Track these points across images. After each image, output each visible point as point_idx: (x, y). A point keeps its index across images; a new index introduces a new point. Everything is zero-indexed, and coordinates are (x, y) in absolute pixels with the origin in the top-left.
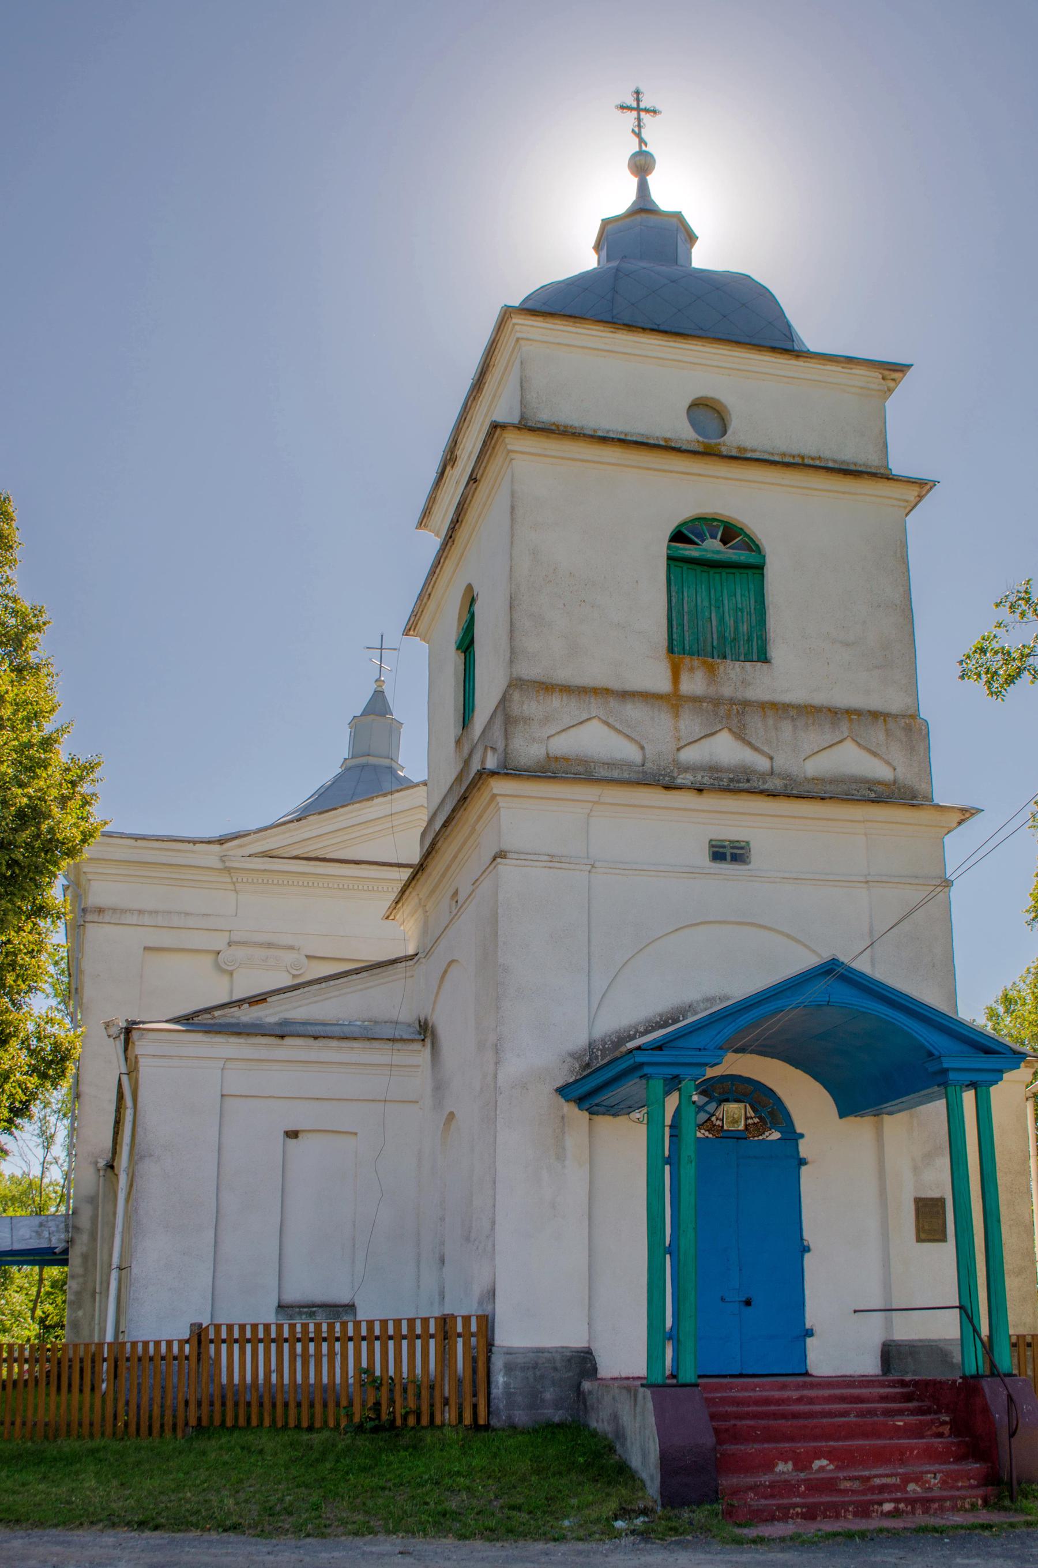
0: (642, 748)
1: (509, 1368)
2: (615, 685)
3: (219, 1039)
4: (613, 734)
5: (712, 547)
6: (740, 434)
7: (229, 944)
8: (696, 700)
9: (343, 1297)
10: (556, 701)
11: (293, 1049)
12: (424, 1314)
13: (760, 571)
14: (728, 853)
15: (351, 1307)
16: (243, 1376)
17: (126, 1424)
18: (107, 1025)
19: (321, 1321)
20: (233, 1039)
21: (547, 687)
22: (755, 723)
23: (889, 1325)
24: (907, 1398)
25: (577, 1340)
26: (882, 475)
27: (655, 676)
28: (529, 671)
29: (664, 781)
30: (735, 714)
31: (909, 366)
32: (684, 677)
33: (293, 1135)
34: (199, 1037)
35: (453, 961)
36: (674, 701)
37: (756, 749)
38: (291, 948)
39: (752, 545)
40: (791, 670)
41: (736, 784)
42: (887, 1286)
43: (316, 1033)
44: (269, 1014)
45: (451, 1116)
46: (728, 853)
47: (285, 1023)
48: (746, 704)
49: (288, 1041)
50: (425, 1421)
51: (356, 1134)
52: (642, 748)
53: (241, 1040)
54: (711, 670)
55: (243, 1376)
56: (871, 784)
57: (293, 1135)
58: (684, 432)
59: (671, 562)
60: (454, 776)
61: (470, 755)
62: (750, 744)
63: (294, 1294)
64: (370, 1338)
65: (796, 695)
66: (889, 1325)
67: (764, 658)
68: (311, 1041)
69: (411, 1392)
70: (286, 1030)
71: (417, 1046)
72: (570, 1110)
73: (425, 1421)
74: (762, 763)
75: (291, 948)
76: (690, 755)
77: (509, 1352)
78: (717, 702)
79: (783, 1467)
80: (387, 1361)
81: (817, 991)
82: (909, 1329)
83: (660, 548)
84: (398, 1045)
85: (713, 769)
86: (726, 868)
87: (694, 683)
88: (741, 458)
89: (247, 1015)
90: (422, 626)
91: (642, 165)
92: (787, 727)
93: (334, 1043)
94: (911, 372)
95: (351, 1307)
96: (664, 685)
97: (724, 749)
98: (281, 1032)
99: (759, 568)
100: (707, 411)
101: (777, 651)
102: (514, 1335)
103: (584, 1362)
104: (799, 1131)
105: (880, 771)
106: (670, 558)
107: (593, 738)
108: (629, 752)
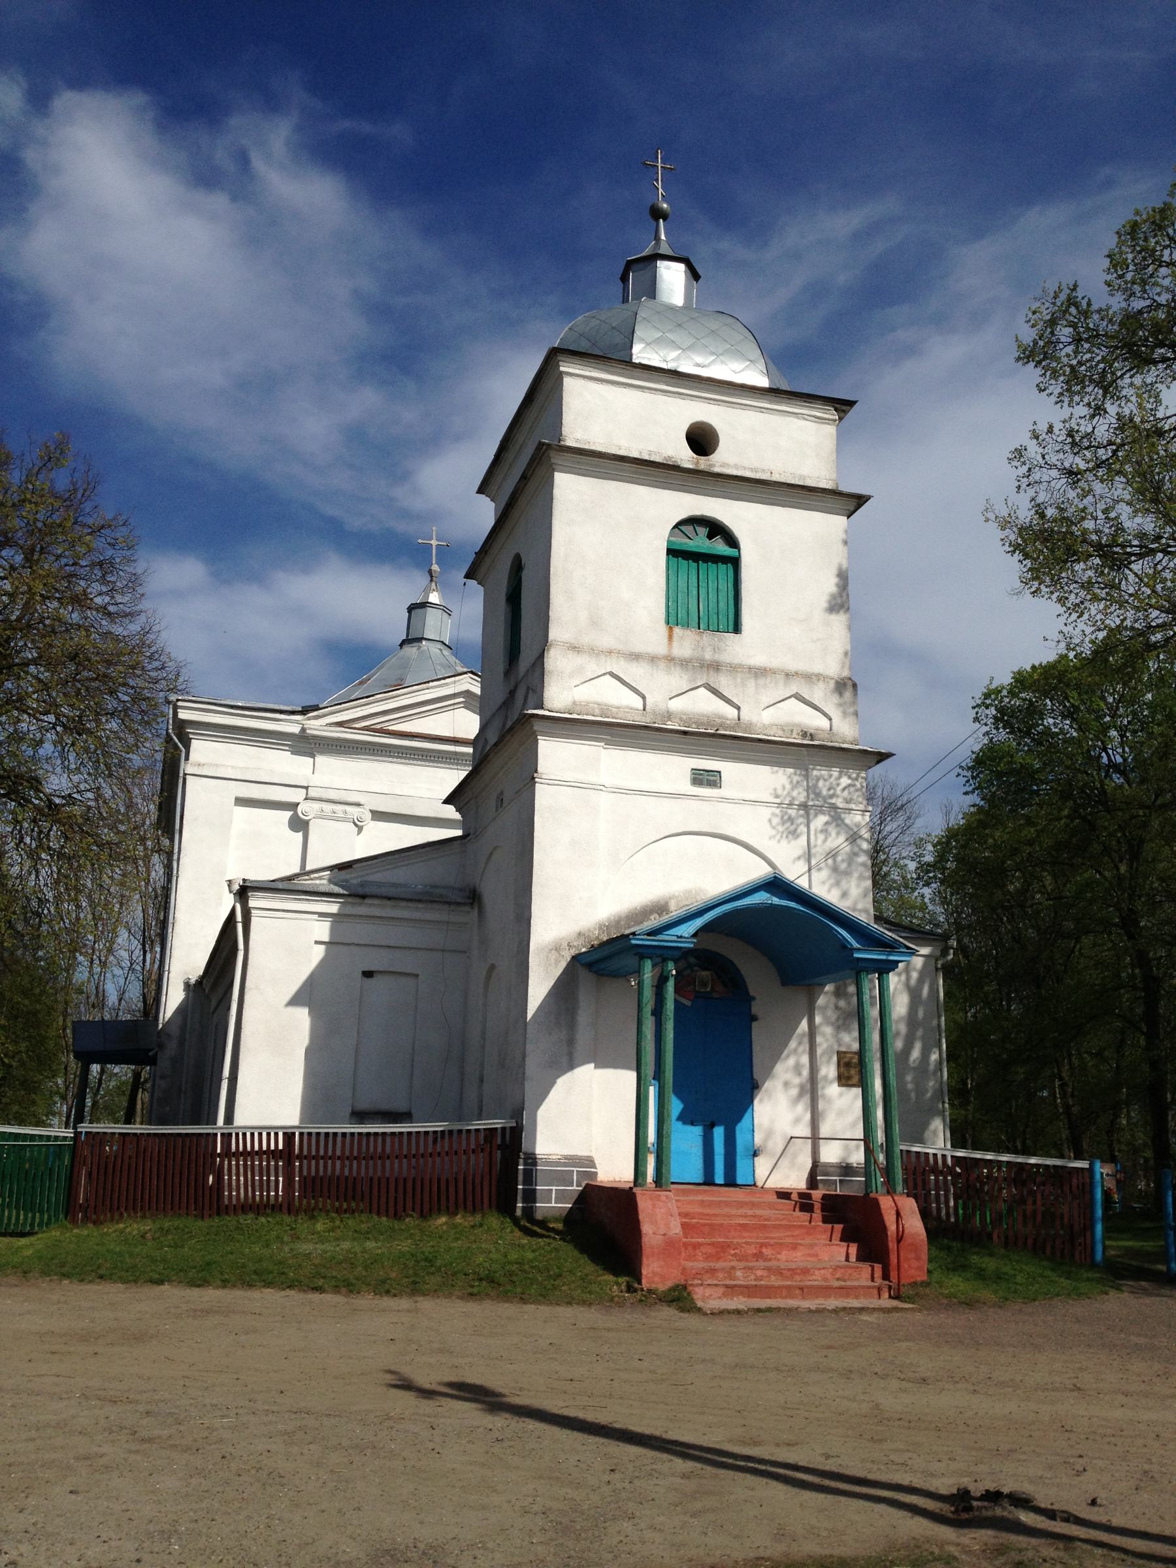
0: (644, 698)
5: (700, 542)
6: (724, 459)
7: (306, 799)
13: (731, 628)
14: (705, 779)
18: (230, 883)
22: (724, 683)
30: (707, 670)
31: (855, 402)
32: (675, 644)
35: (495, 848)
38: (358, 805)
39: (732, 542)
45: (492, 967)
49: (368, 901)
51: (417, 976)
52: (644, 698)
55: (359, 1172)
57: (368, 974)
58: (685, 456)
59: (673, 560)
60: (502, 700)
61: (516, 687)
63: (363, 1105)
65: (759, 659)
70: (367, 890)
71: (467, 908)
75: (358, 805)
76: (676, 705)
80: (227, 1101)
81: (762, 897)
84: (452, 907)
87: (687, 643)
90: (481, 572)
92: (751, 683)
93: (403, 904)
94: (856, 407)
97: (701, 705)
99: (735, 562)
100: (701, 439)
104: (752, 994)
106: (672, 552)
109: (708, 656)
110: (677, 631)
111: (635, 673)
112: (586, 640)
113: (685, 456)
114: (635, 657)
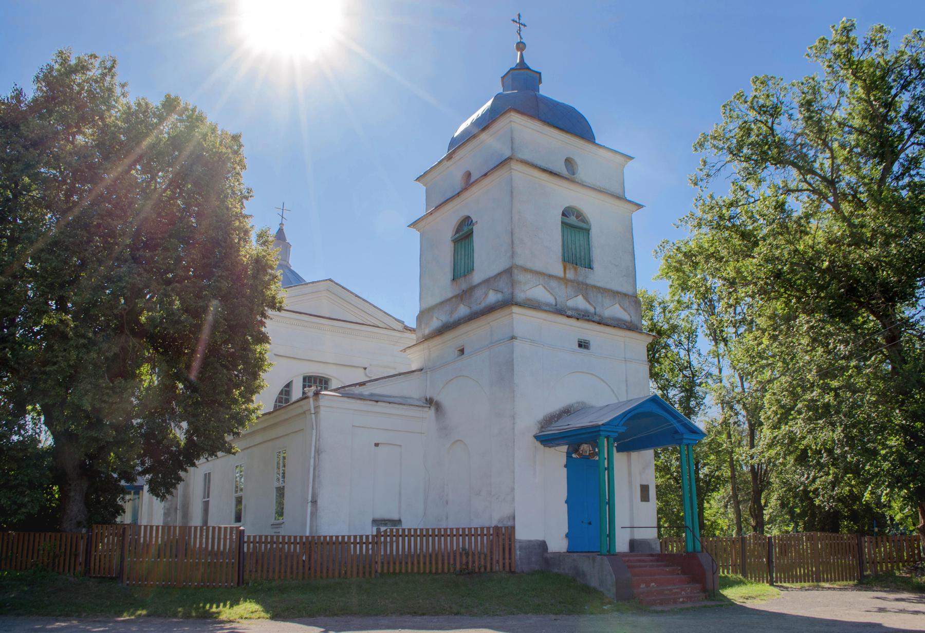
1: (521, 548)
2: (547, 272)
3: (353, 401)
4: (547, 293)
5: (572, 220)
6: (582, 173)
8: (572, 281)
9: (396, 517)
10: (529, 276)
11: (381, 407)
12: (421, 527)
15: (400, 521)
16: (421, 548)
17: (346, 573)
19: (388, 527)
20: (359, 401)
21: (526, 270)
23: (632, 533)
24: (657, 561)
25: (540, 538)
26: (621, 198)
27: (557, 269)
28: (519, 261)
29: (560, 311)
30: (584, 289)
32: (567, 272)
33: (377, 445)
34: (346, 399)
36: (564, 280)
37: (590, 303)
39: (585, 221)
40: (600, 275)
41: (583, 316)
42: (632, 519)
43: (375, 399)
44: (365, 390)
46: (583, 345)
47: (372, 395)
48: (587, 285)
49: (379, 403)
50: (488, 569)
53: (362, 402)
54: (576, 269)
55: (421, 548)
56: (624, 322)
57: (377, 445)
62: (589, 302)
64: (434, 536)
65: (600, 284)
66: (632, 533)
67: (591, 268)
68: (374, 403)
69: (482, 557)
72: (538, 444)
73: (488, 569)
74: (592, 310)
76: (570, 303)
77: (520, 542)
78: (579, 283)
79: (643, 586)
81: (655, 409)
82: (640, 535)
83: (559, 218)
85: (577, 310)
86: (582, 350)
87: (570, 275)
88: (582, 185)
89: (357, 390)
91: (521, 46)
92: (599, 296)
93: (396, 406)
95: (400, 521)
96: (561, 274)
97: (579, 302)
98: (375, 399)
99: (587, 231)
101: (595, 265)
102: (523, 534)
103: (543, 545)
105: (625, 316)
106: (563, 223)
107: (539, 292)
108: (550, 299)
109: (581, 279)
110: (568, 266)
111: (554, 283)
112: (529, 265)
113: (563, 170)
114: (551, 276)
